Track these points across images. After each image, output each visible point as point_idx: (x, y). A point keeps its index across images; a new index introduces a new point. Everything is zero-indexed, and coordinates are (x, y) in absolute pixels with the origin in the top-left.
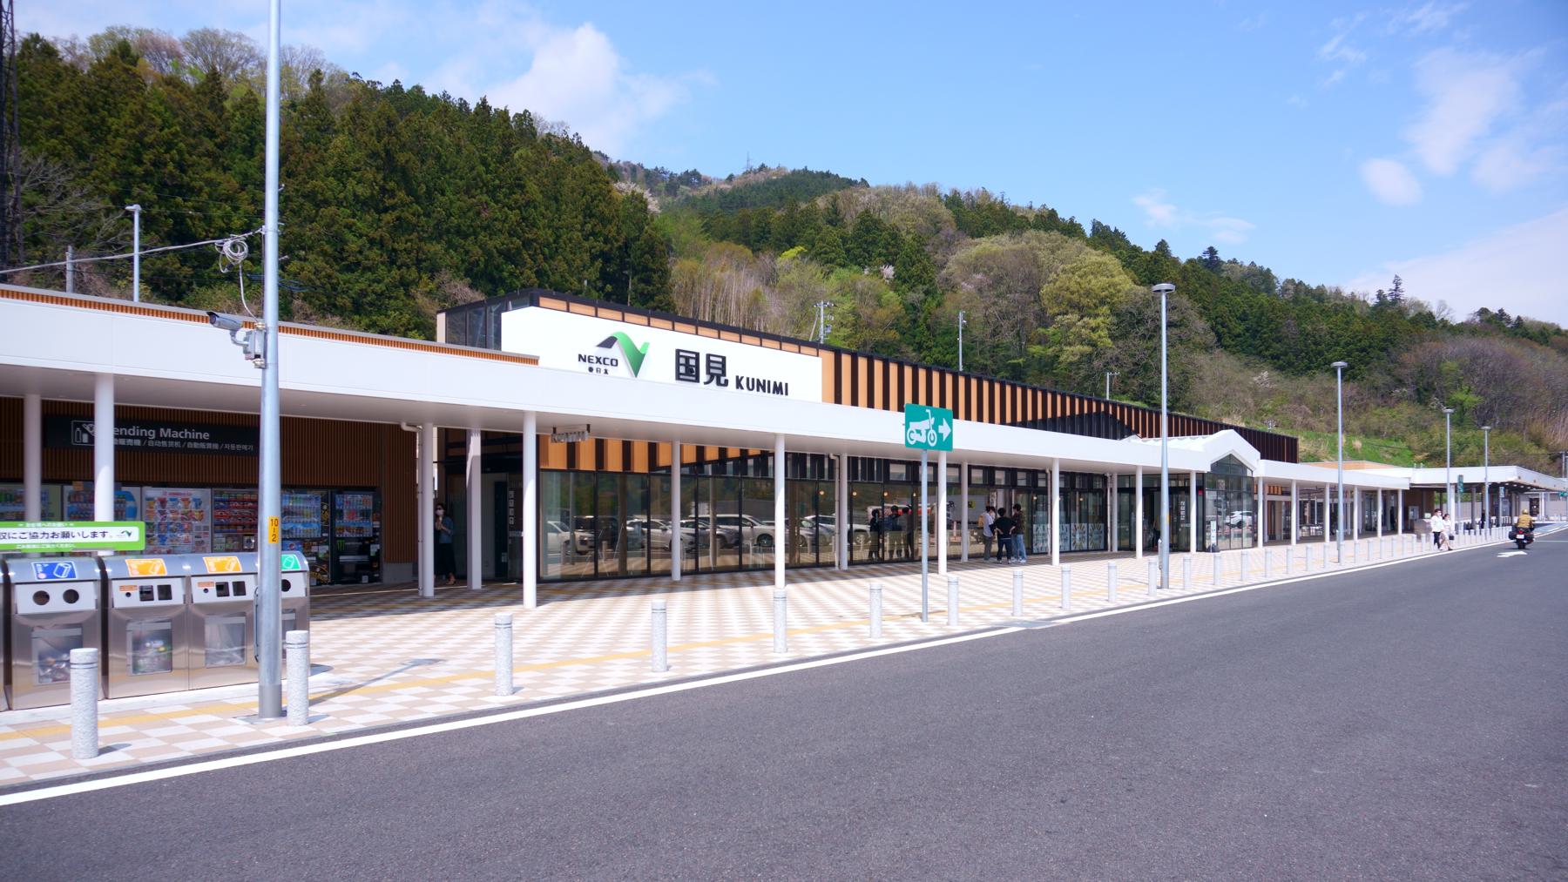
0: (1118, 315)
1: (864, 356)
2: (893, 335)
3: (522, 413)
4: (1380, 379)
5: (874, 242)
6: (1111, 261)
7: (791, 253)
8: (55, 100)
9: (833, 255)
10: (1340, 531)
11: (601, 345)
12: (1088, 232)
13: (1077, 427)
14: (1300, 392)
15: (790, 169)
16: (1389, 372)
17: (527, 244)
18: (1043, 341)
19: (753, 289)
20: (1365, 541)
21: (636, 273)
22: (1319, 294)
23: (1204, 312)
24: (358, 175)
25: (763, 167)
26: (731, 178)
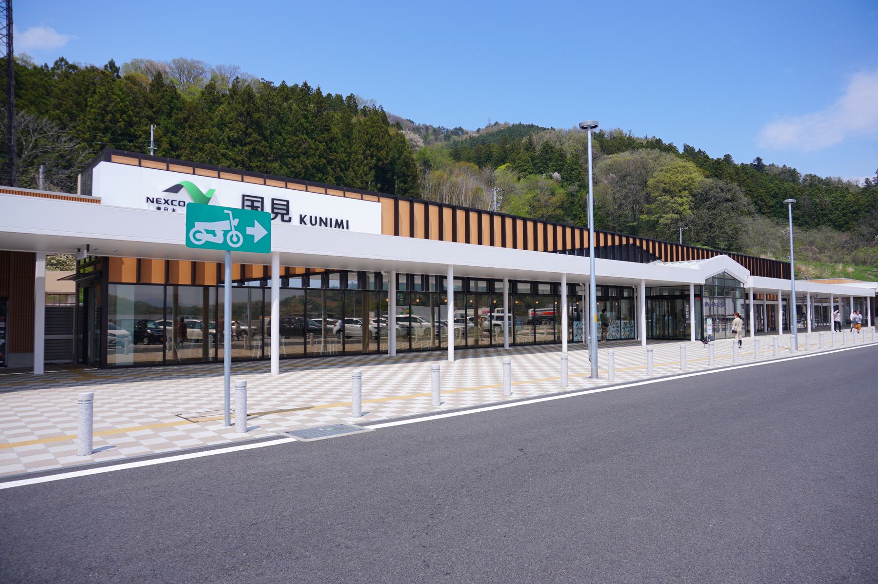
0: (694, 196)
1: (578, 228)
2: (560, 212)
3: (561, 274)
4: (865, 229)
5: (550, 159)
6: (691, 165)
7: (503, 167)
8: (60, 89)
9: (525, 167)
10: (795, 325)
11: (168, 191)
12: (681, 151)
13: (625, 254)
14: (811, 239)
15: (511, 124)
16: (872, 225)
17: (330, 162)
18: (649, 213)
19: (474, 187)
20: (816, 334)
21: (398, 178)
22: (828, 182)
23: (749, 192)
24: (231, 126)
25: (496, 123)
26: (479, 130)
